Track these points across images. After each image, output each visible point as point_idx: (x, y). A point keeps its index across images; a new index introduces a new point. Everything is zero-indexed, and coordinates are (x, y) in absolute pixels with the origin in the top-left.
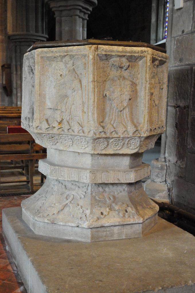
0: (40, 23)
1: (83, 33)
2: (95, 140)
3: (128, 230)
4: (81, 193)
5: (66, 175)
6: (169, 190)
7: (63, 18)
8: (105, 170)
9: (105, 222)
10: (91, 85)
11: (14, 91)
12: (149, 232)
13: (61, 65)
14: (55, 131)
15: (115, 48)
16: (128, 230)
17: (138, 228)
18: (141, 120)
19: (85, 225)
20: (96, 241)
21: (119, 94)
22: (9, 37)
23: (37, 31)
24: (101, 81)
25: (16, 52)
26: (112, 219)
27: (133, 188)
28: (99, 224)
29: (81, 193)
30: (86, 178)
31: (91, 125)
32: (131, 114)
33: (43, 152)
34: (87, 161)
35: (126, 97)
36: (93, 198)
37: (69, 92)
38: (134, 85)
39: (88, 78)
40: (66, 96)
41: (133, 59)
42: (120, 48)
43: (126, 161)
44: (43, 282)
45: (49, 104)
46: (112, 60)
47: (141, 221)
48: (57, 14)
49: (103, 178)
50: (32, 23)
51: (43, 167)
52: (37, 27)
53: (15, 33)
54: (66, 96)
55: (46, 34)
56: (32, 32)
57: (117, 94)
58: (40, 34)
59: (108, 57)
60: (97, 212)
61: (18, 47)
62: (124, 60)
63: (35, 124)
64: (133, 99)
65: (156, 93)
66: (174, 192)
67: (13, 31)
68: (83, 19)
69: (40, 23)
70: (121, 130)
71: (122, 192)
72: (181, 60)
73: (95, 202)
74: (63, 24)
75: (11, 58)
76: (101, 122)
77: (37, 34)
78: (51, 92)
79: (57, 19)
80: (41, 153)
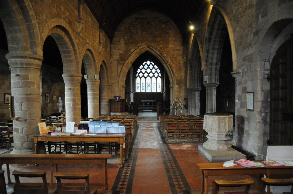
0: (199, 84)
1: (215, 93)
2: (218, 132)
3: (224, 149)
4: (215, 142)
5: (212, 138)
6: (236, 143)
7: (208, 89)
8: (220, 137)
9: (220, 147)
10: (217, 123)
11: (189, 108)
12: (229, 149)
13: (212, 118)
14: (211, 130)
15: (221, 116)
16: (224, 149)
17: (227, 149)
18: (227, 129)
19: (216, 147)
20: (218, 150)
21: (222, 124)
22: (187, 89)
23: (198, 87)
24: (219, 122)
25: (190, 94)
26: (221, 147)
27: (226, 141)
28: (219, 147)
29: (215, 142)
30: (216, 139)
31: (217, 130)
32: (225, 128)
33: (207, 134)
34: (216, 136)
35: (224, 124)
36: (218, 143)
37: (213, 123)
38: (225, 122)
39: (217, 121)
40: (213, 124)
41: (225, 118)
42: (222, 116)
43: (224, 136)
44: (209, 154)
45: (209, 125)
46: (221, 118)
47: (227, 147)
48: (206, 88)
49: (219, 139)
50: (196, 84)
51: (207, 136)
52: (197, 85)
53: (190, 88)
54: (213, 124)
55: (200, 87)
56: (196, 87)
57: (222, 124)
58: (198, 88)
59: (220, 118)
60: (218, 145)
61: (191, 92)
62: (223, 118)
63: (207, 129)
64: (225, 125)
65: (230, 123)
66: (237, 143)
67: (189, 87)
68: (215, 89)
69: (199, 84)
70: (223, 130)
71: (223, 142)
72: (238, 113)
73: (218, 143)
74: (208, 90)
75: (188, 96)
76: (219, 129)
77: (197, 88)
78: (210, 123)
79: (206, 89)
80: (79, 96)
